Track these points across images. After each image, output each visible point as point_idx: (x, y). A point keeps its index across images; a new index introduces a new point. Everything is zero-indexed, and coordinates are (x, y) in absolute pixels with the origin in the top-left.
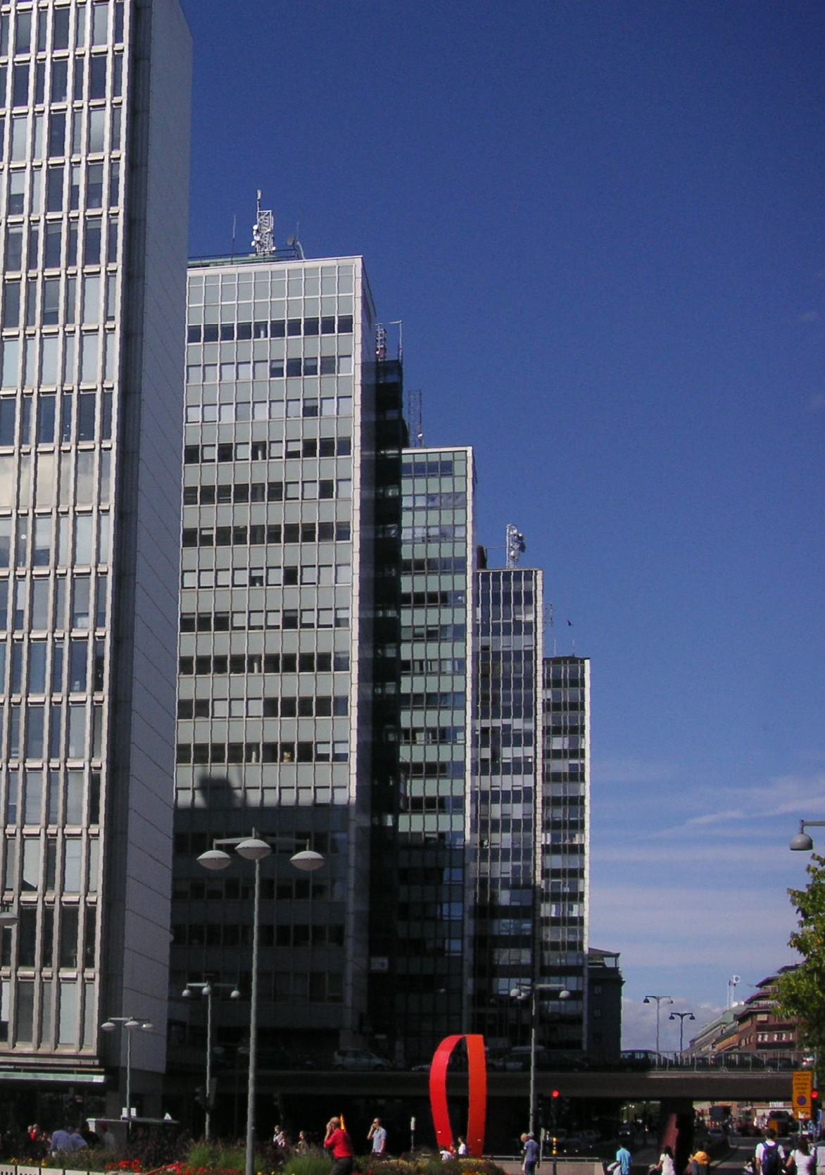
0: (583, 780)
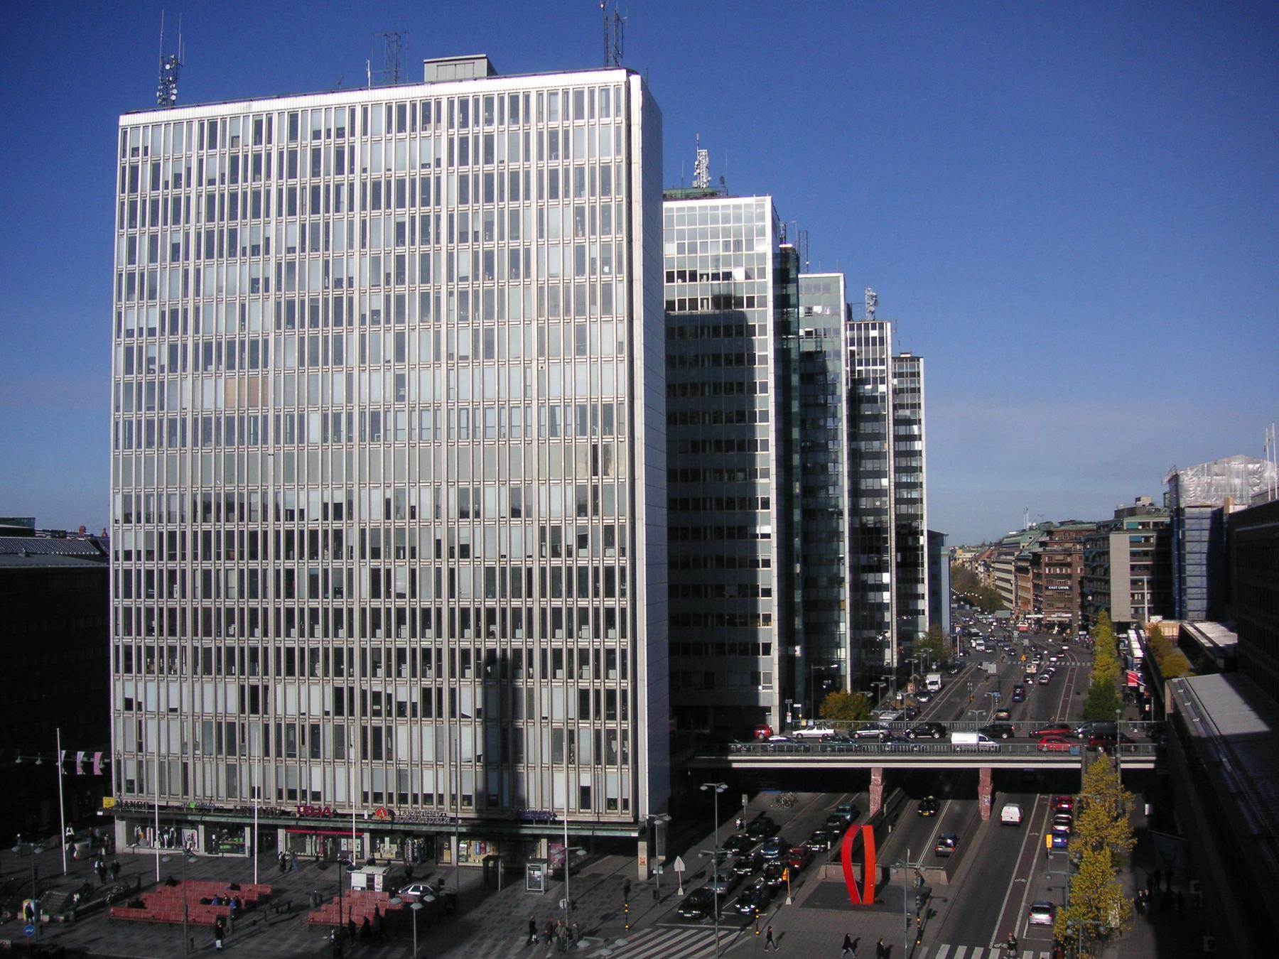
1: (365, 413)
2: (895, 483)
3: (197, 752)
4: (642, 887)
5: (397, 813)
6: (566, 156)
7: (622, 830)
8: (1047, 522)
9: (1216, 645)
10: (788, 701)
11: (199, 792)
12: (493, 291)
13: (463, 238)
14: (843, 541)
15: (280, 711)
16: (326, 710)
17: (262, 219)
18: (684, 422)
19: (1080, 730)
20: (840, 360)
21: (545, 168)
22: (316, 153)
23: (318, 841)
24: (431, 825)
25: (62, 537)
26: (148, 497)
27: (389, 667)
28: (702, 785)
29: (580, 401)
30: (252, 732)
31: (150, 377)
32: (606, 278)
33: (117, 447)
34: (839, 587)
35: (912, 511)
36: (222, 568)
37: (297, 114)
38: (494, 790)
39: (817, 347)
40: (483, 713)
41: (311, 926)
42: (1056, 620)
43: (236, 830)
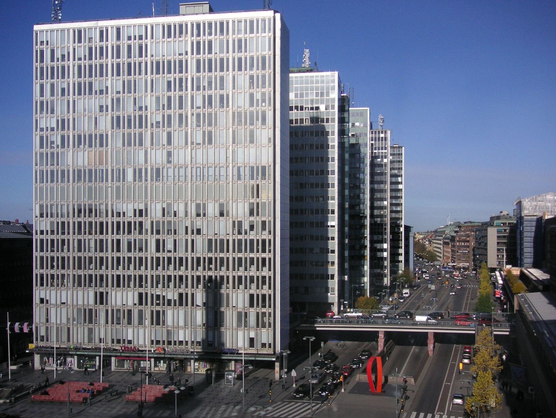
1: (153, 168)
2: (390, 203)
3: (74, 322)
4: (277, 383)
5: (167, 349)
6: (246, 51)
7: (268, 357)
8: (458, 222)
9: (538, 279)
10: (342, 300)
11: (75, 340)
12: (212, 113)
13: (198, 89)
14: (367, 229)
15: (113, 303)
16: (135, 303)
17: (104, 78)
18: (296, 174)
19: (474, 316)
20: (367, 147)
21: (236, 57)
22: (129, 47)
23: (130, 363)
24: (182, 355)
25: (8, 224)
26: (51, 205)
27: (164, 283)
28: (304, 337)
29: (251, 165)
30: (100, 313)
31: (52, 150)
32: (263, 109)
33: (36, 182)
34: (364, 250)
35: (397, 216)
36: (87, 238)
37: (120, 28)
38: (211, 339)
39: (356, 141)
40: (206, 304)
41: (127, 402)
42: (462, 266)
43: (93, 358)
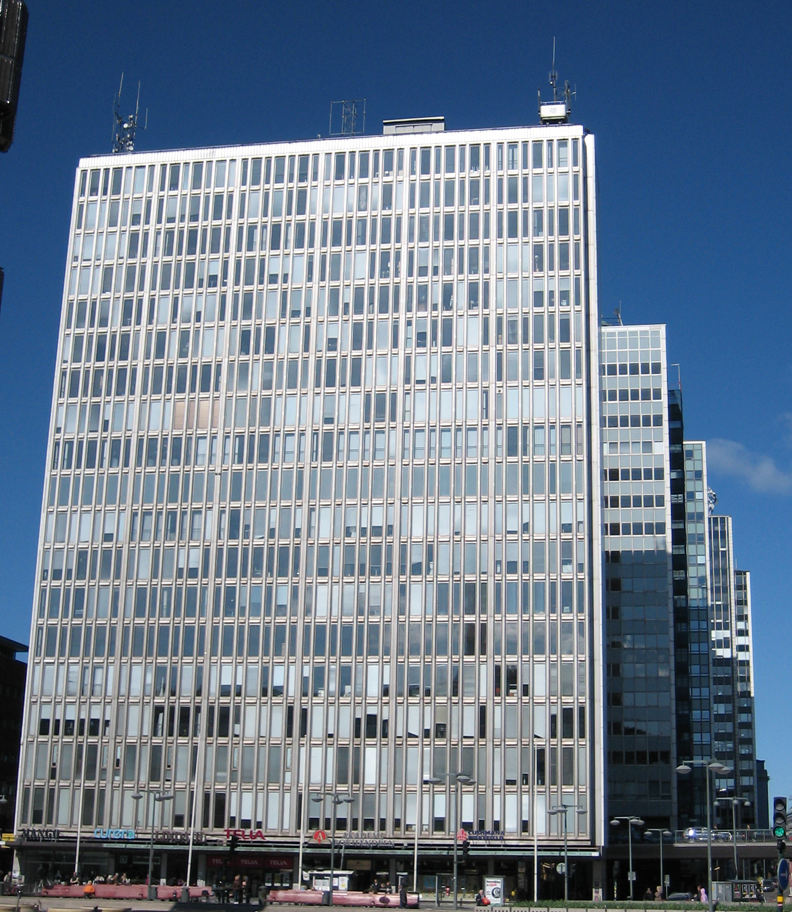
0: (746, 604)
3: (117, 778)
